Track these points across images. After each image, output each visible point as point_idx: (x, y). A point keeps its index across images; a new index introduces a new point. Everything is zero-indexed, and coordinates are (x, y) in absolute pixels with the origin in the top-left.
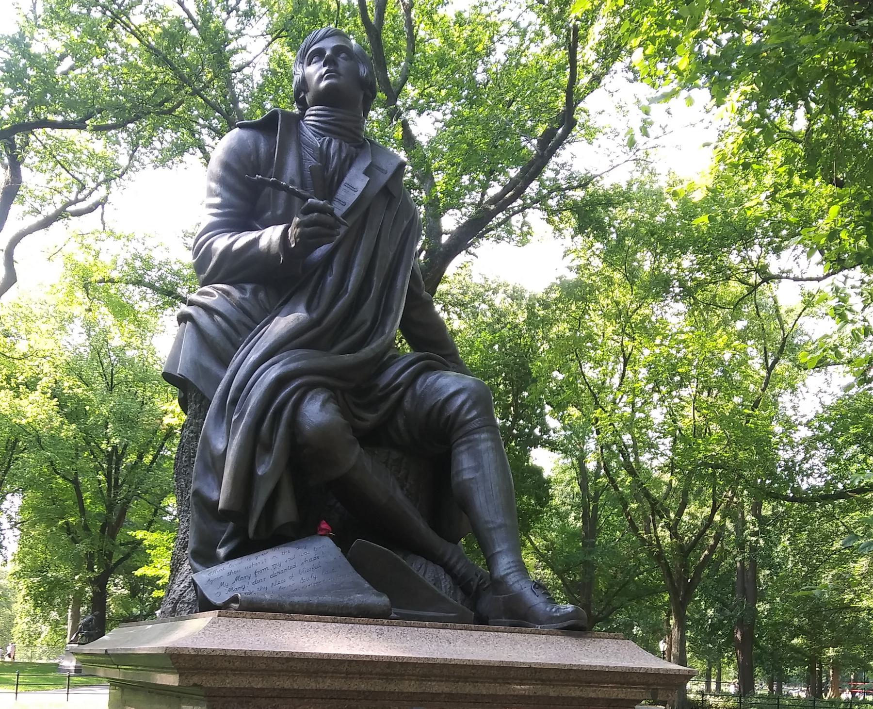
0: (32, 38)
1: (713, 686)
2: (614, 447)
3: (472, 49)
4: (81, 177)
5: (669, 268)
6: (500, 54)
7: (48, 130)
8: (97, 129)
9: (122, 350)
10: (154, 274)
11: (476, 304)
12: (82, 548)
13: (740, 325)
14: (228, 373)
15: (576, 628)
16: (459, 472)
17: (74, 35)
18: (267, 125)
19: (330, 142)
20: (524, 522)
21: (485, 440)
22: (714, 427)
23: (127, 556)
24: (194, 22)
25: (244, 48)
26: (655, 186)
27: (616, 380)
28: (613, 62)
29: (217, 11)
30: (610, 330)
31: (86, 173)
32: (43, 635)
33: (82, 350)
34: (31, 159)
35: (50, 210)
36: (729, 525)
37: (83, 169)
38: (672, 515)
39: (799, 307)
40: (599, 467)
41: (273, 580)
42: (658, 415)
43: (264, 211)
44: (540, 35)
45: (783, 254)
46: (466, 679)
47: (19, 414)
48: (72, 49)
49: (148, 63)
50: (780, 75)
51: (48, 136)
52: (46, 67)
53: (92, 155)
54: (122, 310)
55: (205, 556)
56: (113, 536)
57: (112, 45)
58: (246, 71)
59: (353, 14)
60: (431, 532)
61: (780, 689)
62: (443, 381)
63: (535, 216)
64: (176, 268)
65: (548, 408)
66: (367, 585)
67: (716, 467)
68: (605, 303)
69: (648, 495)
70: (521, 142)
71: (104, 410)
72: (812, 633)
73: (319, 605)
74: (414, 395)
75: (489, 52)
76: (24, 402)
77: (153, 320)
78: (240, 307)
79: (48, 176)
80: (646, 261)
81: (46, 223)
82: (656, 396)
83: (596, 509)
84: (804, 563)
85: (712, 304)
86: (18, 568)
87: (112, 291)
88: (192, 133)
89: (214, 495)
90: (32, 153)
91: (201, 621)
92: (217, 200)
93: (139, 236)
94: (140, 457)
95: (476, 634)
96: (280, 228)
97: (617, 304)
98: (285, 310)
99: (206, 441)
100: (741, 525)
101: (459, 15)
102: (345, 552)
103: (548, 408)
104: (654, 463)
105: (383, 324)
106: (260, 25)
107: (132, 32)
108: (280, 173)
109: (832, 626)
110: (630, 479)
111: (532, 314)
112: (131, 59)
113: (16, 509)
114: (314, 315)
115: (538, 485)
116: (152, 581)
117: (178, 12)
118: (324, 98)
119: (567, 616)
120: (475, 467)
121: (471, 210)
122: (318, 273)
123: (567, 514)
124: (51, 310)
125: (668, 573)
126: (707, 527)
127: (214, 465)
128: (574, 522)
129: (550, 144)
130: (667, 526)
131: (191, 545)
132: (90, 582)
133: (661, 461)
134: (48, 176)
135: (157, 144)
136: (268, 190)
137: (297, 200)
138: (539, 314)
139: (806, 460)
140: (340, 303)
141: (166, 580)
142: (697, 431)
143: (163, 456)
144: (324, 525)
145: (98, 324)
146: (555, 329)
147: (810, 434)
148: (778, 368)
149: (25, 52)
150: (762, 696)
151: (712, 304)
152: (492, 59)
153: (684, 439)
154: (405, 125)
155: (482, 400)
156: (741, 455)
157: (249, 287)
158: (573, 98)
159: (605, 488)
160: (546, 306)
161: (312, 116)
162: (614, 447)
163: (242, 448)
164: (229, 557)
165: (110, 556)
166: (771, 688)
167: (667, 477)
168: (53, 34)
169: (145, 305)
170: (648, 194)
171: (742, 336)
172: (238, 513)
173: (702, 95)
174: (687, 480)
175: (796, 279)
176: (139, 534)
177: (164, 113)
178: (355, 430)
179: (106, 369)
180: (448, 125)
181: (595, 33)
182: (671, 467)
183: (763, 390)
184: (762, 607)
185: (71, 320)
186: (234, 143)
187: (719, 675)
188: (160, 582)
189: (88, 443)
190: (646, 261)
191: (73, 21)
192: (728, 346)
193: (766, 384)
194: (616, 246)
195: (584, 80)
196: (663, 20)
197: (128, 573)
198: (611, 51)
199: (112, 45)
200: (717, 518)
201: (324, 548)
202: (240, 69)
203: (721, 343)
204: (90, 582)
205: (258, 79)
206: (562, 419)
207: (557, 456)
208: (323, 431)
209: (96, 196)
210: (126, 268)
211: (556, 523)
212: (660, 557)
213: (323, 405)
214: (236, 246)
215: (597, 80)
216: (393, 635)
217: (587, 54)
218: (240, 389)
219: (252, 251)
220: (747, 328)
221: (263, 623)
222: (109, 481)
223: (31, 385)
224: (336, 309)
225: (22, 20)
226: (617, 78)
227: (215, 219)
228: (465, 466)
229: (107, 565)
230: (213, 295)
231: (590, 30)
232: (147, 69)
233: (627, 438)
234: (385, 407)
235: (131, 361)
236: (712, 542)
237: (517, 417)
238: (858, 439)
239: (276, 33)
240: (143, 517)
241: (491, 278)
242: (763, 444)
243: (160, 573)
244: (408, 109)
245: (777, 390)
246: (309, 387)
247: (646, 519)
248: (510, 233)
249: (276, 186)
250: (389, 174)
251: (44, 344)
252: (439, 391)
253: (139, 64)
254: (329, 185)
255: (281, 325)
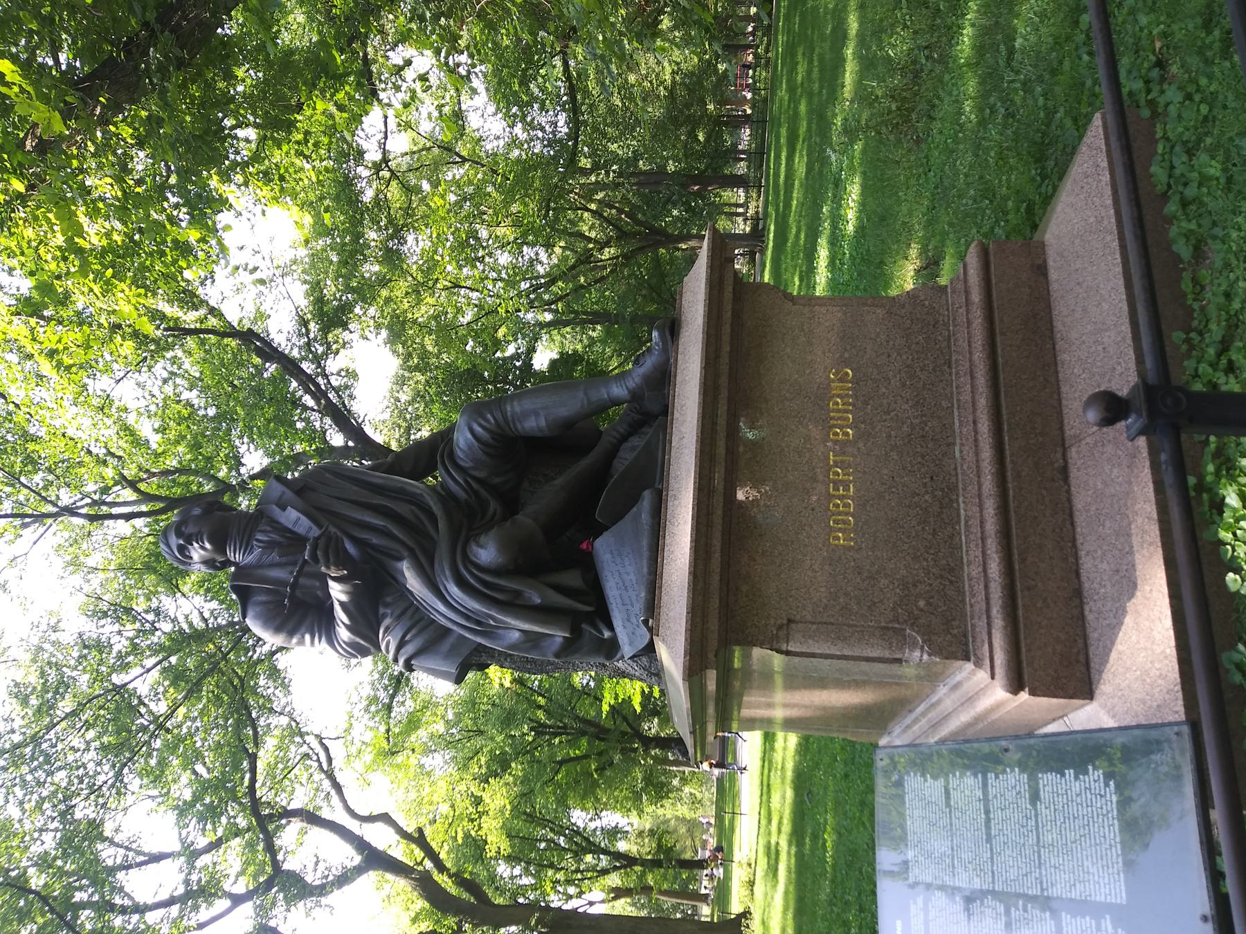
0: (179, 799)
1: (741, 210)
2: (532, 296)
3: (185, 419)
4: (298, 757)
5: (374, 250)
6: (192, 396)
7: (257, 785)
8: (256, 744)
9: (447, 722)
10: (382, 695)
11: (408, 416)
12: (617, 758)
13: (426, 186)
14: (455, 628)
15: (673, 329)
16: (540, 430)
17: (175, 762)
18: (245, 596)
19: (258, 540)
20: (597, 374)
21: (512, 407)
22: (515, 208)
23: (625, 719)
24: (165, 659)
25: (187, 617)
26: (307, 260)
27: (475, 295)
28: (197, 297)
29: (155, 640)
30: (431, 301)
31: (294, 752)
32: (693, 791)
33: (447, 757)
34: (282, 800)
35: (327, 784)
36: (600, 196)
37: (292, 756)
38: (591, 246)
39: (410, 133)
40: (550, 311)
41: (630, 590)
42: (504, 258)
43: (317, 597)
44: (174, 360)
45: (365, 148)
46: (714, 424)
47: (502, 811)
48: (187, 764)
49: (200, 699)
50: (203, 149)
51: (263, 785)
52: (204, 788)
53: (280, 748)
54: (413, 723)
55: (611, 648)
56: (608, 731)
57: (185, 730)
58: (207, 615)
59: (157, 522)
60: (591, 454)
61: (743, 152)
62: (462, 443)
63: (332, 365)
64: (377, 676)
65: (499, 354)
66: (635, 509)
67: (548, 206)
68: (407, 305)
69: (573, 267)
70: (266, 377)
71: (499, 738)
72: (694, 124)
73: (650, 550)
74: (474, 468)
75: (189, 404)
76: (492, 806)
77: (422, 696)
78: (398, 618)
79: (297, 786)
80: (371, 269)
81: (337, 787)
82: (487, 259)
83: (585, 313)
84: (633, 129)
85: (408, 211)
86: (635, 813)
87: (397, 730)
88: (260, 661)
89: (559, 640)
90: (278, 799)
91: (662, 651)
92: (307, 637)
93: (349, 708)
94: (540, 707)
95: (676, 415)
96: (331, 583)
97: (407, 293)
98: (401, 579)
99: (513, 647)
100: (599, 186)
101: (156, 431)
102: (607, 528)
103: (499, 354)
104: (546, 260)
105: (414, 495)
106: (167, 603)
107: (173, 712)
108: (284, 583)
109: (688, 106)
110: (560, 283)
111: (417, 368)
112: (196, 714)
113: (584, 814)
114: (406, 554)
115: (564, 363)
116: (647, 698)
117: (155, 673)
118: (220, 545)
119: (662, 336)
120: (535, 417)
121: (328, 421)
122: (370, 551)
123: (590, 338)
124: (413, 783)
125: (641, 249)
126: (601, 216)
127: (532, 640)
128: (597, 332)
129: (269, 352)
130: (601, 250)
131: (602, 660)
132: (646, 751)
133: (543, 256)
134: (297, 786)
135: (270, 691)
136: (298, 593)
137: (306, 569)
138: (416, 361)
139: (542, 129)
140: (395, 532)
141: (644, 685)
142: (517, 224)
143: (539, 687)
144: (584, 546)
145: (425, 743)
146: (430, 348)
147: (520, 125)
148: (464, 153)
149: (191, 804)
150: (748, 167)
151: (408, 211)
152: (196, 402)
153: (524, 235)
154: (253, 477)
155: (476, 410)
156: (537, 184)
157: (382, 610)
158: (232, 332)
159: (568, 305)
160: (409, 356)
161: (236, 556)
162: (532, 296)
163: (517, 616)
164: (611, 627)
165: (624, 734)
166: (742, 159)
167: (557, 250)
168: (174, 781)
169: (409, 703)
170: (313, 265)
171: (435, 184)
172: (575, 622)
173: (223, 218)
174: (564, 233)
175: (386, 138)
176: (605, 708)
177: (242, 685)
178: (504, 519)
179: (465, 737)
180: (253, 441)
181: (171, 311)
182: (549, 246)
183: (483, 166)
184: (671, 167)
185: (422, 766)
186: (258, 623)
187: (731, 205)
188: (647, 690)
189: (528, 752)
190: (371, 269)
191: (163, 764)
192: (443, 197)
193: (477, 163)
194: (358, 294)
195: (213, 322)
196: (157, 252)
197: (639, 718)
198: (189, 299)
199: (185, 730)
200: (593, 207)
201: (603, 547)
202: (205, 620)
203: (440, 202)
204: (646, 751)
205: (214, 605)
206: (508, 342)
207: (540, 347)
208: (503, 547)
209: (315, 744)
210: (377, 719)
211: (598, 348)
212: (625, 256)
213: (481, 547)
214: (346, 621)
215: (212, 311)
216: (676, 486)
217: (190, 318)
218: (468, 618)
219: (352, 608)
220: (429, 180)
221: (664, 598)
222: (561, 734)
223: (478, 801)
224: (401, 537)
225: (163, 808)
226: (211, 294)
227: (323, 639)
228: (534, 424)
229: (632, 736)
230: (389, 641)
231: (169, 315)
232: (204, 701)
233: (524, 286)
234: (483, 493)
235: (457, 715)
236: (614, 211)
237: (505, 381)
238: (524, 83)
239: (174, 589)
240: (591, 705)
241: (386, 403)
242: (527, 167)
243: (638, 690)
244: (240, 475)
245: (483, 154)
246: (466, 558)
247: (592, 269)
248: (347, 387)
249: (294, 586)
250: (284, 489)
251: (442, 788)
252: (470, 447)
253: (201, 706)
254: (293, 541)
255: (413, 582)
